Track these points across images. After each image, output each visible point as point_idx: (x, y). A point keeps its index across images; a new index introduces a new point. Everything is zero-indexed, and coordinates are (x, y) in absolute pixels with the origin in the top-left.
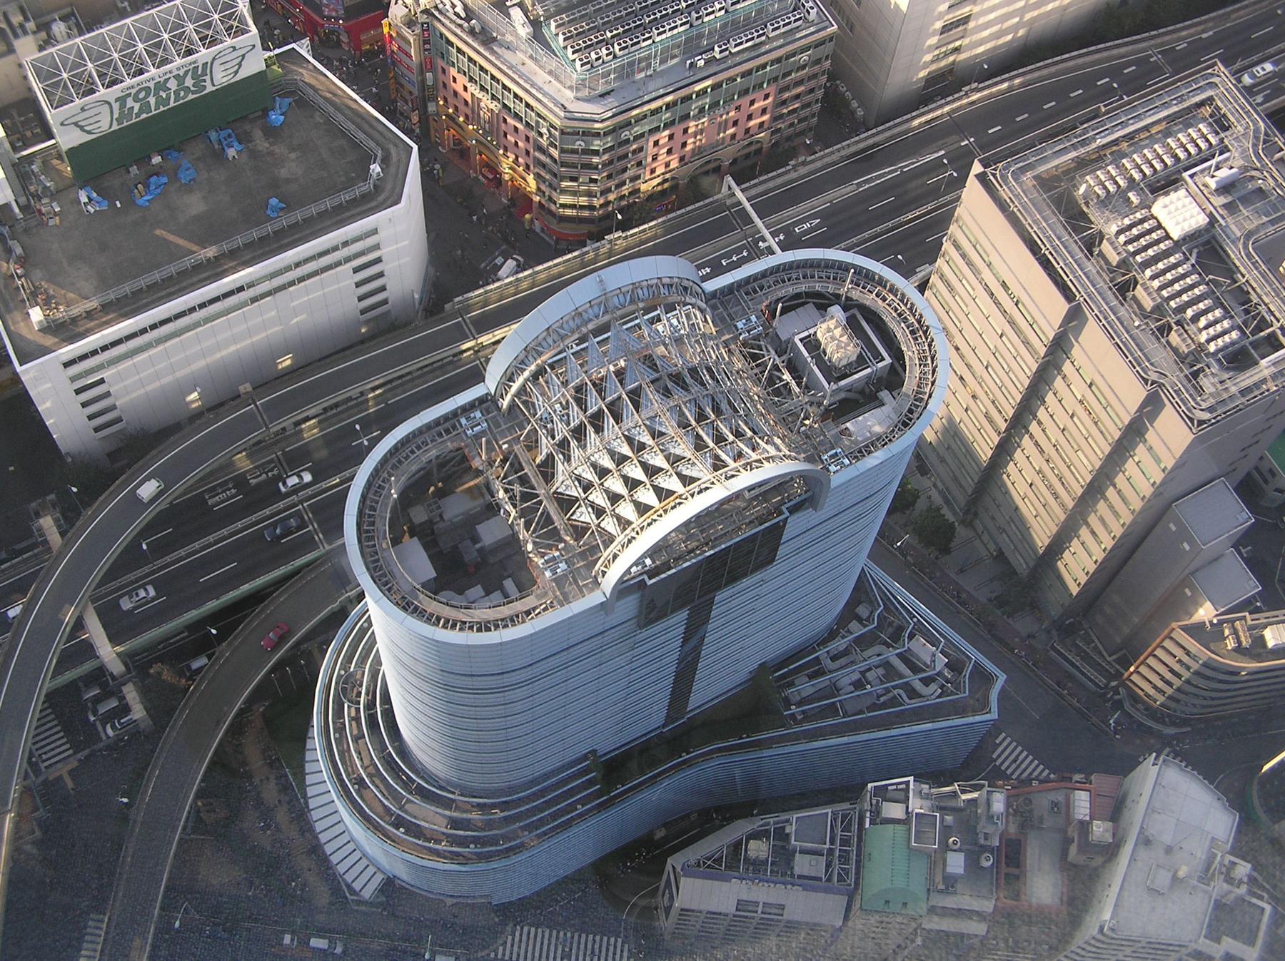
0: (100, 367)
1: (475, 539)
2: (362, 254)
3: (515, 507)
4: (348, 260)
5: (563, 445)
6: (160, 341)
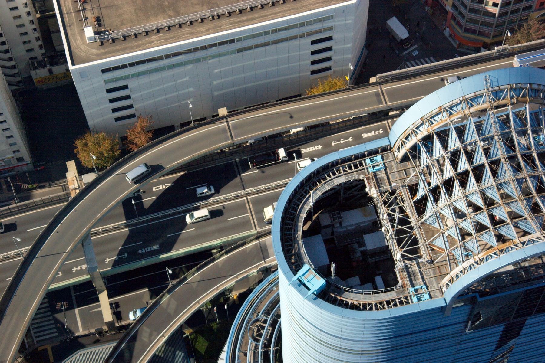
0: (127, 77)
1: (362, 244)
2: (320, 31)
3: (393, 227)
4: (309, 34)
5: (435, 192)
6: (170, 67)
